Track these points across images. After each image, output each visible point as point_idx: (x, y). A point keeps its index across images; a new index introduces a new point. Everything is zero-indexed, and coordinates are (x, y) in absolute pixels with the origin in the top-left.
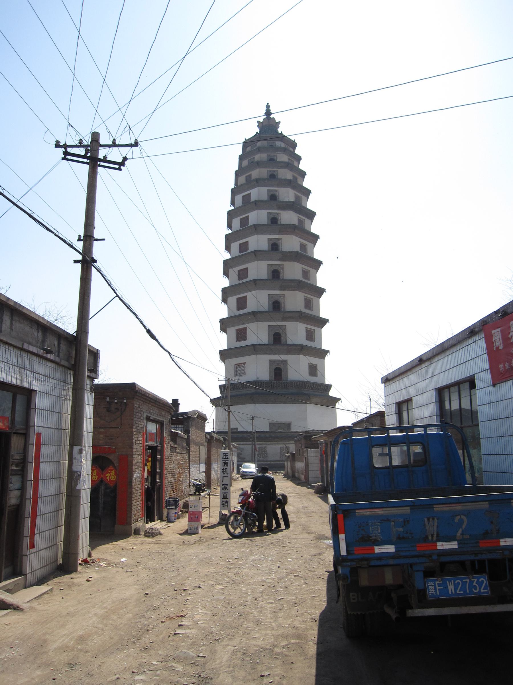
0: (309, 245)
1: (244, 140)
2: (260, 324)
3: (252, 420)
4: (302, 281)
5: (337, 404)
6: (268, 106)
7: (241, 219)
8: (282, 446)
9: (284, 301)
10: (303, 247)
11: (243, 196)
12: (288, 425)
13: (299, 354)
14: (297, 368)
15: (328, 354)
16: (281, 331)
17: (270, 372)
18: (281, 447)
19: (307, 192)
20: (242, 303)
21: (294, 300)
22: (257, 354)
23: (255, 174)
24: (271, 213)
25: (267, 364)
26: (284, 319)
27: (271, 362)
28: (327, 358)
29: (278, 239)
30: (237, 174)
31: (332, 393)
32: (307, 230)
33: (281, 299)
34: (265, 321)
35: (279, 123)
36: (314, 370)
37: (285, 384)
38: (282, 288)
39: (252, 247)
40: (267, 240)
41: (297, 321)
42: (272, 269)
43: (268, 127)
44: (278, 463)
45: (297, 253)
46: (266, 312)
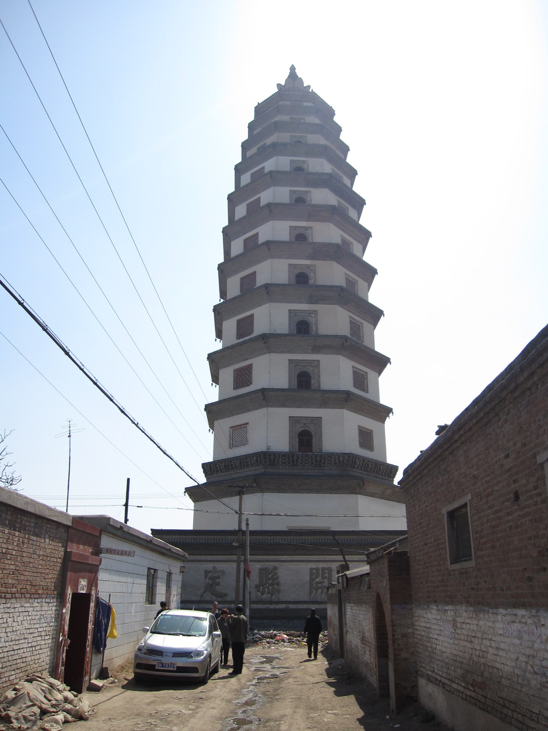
0: (366, 325)
2: (274, 356)
3: (269, 207)
4: (353, 394)
7: (248, 205)
8: (313, 565)
9: (317, 321)
10: (356, 328)
11: (252, 174)
13: (342, 408)
14: (339, 432)
15: (391, 415)
16: (310, 370)
17: (291, 439)
18: (311, 569)
19: (375, 315)
20: (243, 377)
21: (336, 373)
22: (268, 406)
23: (267, 231)
24: (295, 266)
25: (286, 268)
26: (316, 349)
27: (293, 420)
28: (390, 423)
29: (306, 228)
30: (239, 170)
32: (367, 348)
33: (310, 318)
34: (282, 352)
36: (367, 438)
37: (318, 459)
38: (311, 301)
39: (259, 328)
40: (289, 161)
41: (338, 353)
42: (297, 271)
44: (305, 606)
45: (345, 338)
46: (285, 335)
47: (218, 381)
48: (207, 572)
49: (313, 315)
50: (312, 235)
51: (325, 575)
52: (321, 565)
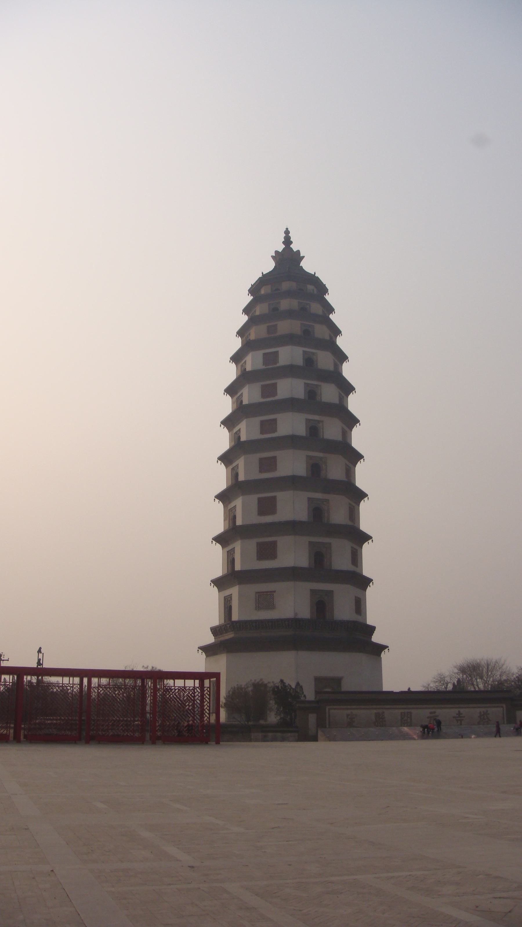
1: (261, 275)
5: (383, 653)
6: (287, 232)
8: (403, 711)
12: (338, 681)
18: (401, 713)
27: (313, 592)
29: (319, 422)
31: (376, 638)
35: (304, 257)
43: (288, 260)
47: (356, 600)
48: (348, 715)
49: (325, 503)
50: (323, 429)
51: (83, 718)
52: (406, 711)
